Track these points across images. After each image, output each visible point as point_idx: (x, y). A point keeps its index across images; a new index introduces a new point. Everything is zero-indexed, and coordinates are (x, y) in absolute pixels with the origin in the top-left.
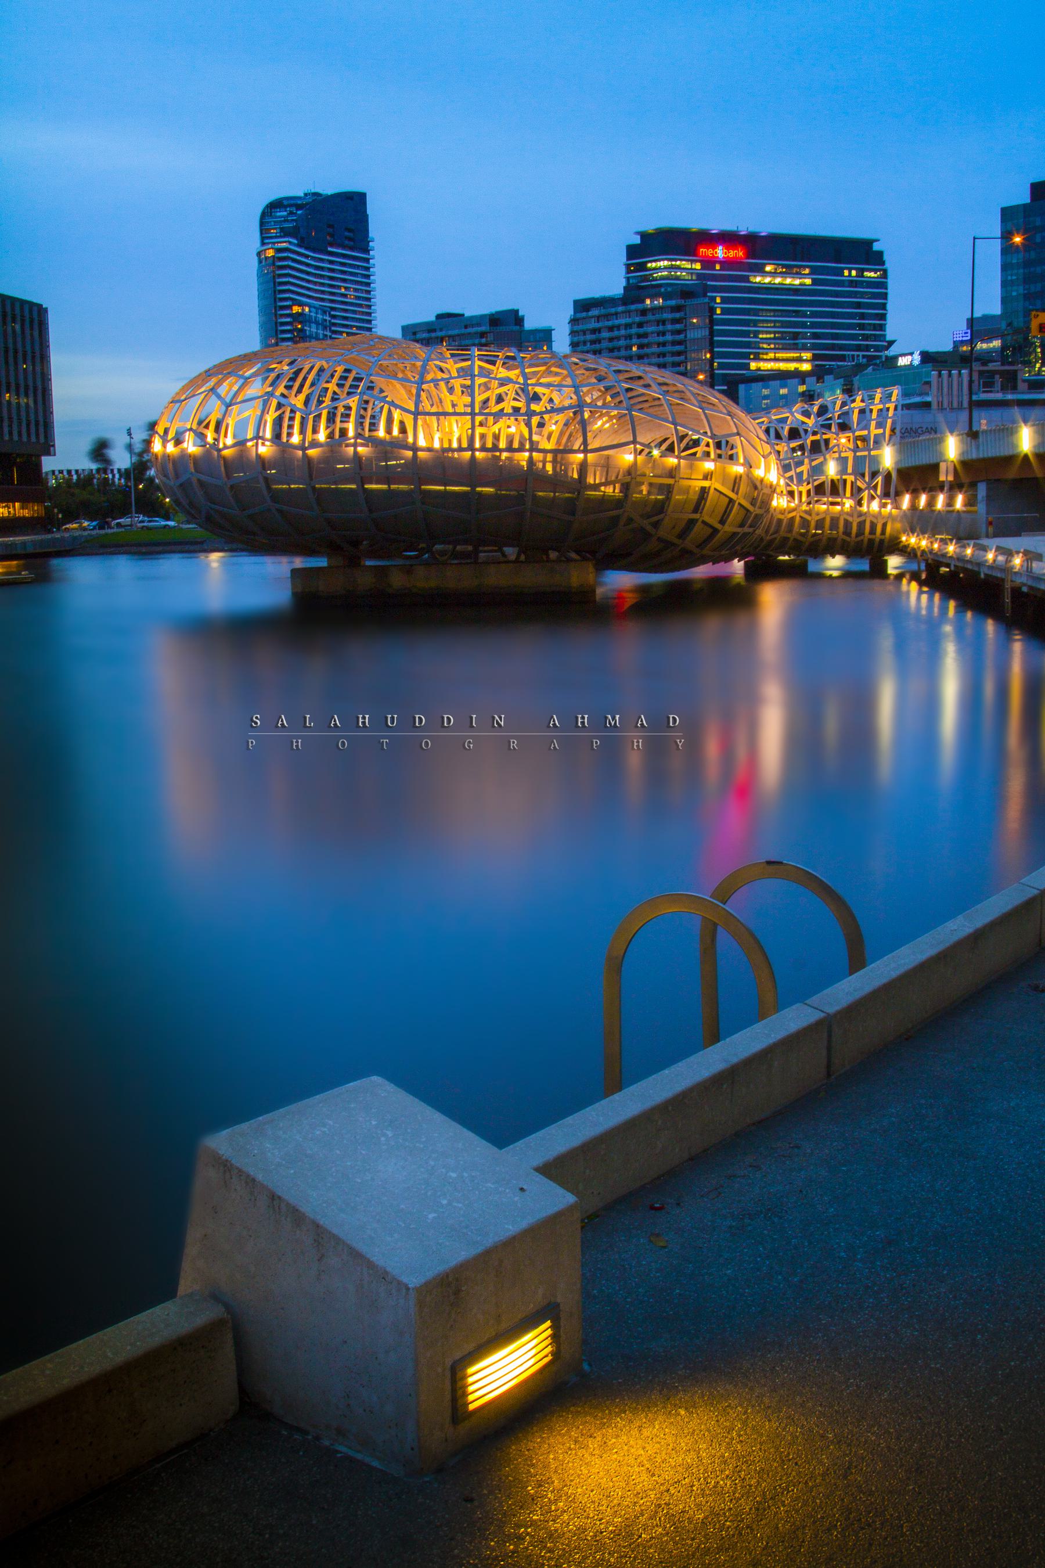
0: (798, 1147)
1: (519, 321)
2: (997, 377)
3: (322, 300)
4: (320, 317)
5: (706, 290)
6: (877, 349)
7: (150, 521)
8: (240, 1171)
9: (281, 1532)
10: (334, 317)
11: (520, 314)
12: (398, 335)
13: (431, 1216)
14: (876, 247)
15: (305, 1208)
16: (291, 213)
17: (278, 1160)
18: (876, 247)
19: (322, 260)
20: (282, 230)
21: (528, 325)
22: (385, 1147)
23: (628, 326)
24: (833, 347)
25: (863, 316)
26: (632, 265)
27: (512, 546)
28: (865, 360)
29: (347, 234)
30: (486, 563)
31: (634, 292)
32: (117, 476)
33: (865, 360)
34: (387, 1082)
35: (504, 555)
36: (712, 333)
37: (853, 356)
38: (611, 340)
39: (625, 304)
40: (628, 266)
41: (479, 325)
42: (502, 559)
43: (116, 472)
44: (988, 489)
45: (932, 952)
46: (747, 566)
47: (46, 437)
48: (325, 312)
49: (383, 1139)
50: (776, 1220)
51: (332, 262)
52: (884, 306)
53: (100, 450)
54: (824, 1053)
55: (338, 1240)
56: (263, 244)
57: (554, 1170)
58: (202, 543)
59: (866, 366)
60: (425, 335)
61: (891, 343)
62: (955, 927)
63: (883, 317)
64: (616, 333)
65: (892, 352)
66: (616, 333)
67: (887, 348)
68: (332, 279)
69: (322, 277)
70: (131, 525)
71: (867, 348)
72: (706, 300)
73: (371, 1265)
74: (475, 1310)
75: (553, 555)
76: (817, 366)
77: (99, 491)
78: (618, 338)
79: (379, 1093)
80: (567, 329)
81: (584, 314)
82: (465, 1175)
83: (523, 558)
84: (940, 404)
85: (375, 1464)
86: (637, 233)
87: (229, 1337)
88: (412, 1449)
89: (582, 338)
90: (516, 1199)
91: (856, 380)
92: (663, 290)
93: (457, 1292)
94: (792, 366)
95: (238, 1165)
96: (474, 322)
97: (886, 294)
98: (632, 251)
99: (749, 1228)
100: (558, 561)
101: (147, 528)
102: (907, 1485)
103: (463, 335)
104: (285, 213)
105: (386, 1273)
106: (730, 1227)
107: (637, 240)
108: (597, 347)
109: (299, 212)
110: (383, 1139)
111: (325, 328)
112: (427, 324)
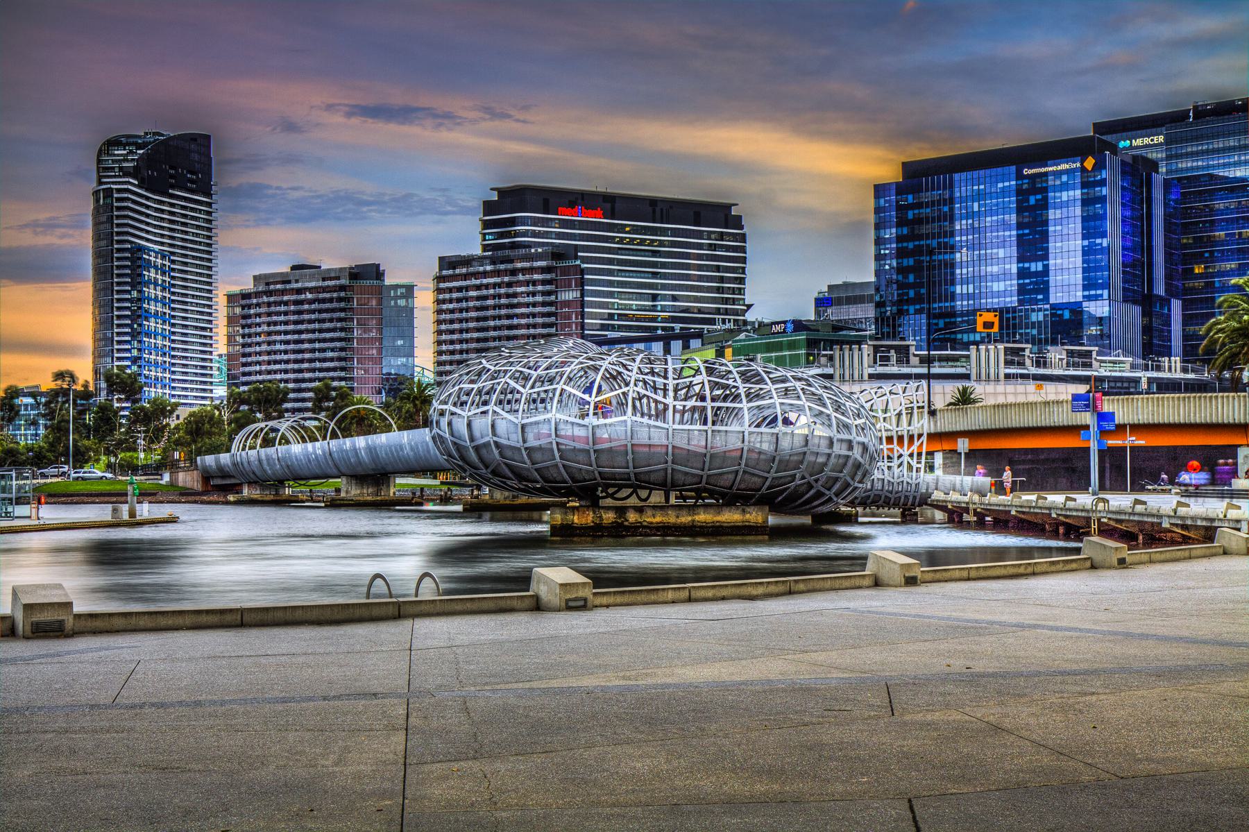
2: (893, 352)
3: (162, 244)
4: (159, 261)
6: (736, 312)
16: (131, 152)
21: (388, 282)
23: (495, 286)
25: (722, 280)
36: (582, 296)
39: (493, 263)
41: (338, 278)
44: (944, 458)
48: (163, 257)
51: (172, 205)
56: (100, 183)
61: (749, 306)
63: (741, 281)
64: (485, 292)
66: (485, 292)
69: (162, 219)
80: (431, 285)
81: (451, 272)
84: (842, 377)
89: (447, 296)
101: (83, 479)
107: (494, 197)
111: (163, 273)
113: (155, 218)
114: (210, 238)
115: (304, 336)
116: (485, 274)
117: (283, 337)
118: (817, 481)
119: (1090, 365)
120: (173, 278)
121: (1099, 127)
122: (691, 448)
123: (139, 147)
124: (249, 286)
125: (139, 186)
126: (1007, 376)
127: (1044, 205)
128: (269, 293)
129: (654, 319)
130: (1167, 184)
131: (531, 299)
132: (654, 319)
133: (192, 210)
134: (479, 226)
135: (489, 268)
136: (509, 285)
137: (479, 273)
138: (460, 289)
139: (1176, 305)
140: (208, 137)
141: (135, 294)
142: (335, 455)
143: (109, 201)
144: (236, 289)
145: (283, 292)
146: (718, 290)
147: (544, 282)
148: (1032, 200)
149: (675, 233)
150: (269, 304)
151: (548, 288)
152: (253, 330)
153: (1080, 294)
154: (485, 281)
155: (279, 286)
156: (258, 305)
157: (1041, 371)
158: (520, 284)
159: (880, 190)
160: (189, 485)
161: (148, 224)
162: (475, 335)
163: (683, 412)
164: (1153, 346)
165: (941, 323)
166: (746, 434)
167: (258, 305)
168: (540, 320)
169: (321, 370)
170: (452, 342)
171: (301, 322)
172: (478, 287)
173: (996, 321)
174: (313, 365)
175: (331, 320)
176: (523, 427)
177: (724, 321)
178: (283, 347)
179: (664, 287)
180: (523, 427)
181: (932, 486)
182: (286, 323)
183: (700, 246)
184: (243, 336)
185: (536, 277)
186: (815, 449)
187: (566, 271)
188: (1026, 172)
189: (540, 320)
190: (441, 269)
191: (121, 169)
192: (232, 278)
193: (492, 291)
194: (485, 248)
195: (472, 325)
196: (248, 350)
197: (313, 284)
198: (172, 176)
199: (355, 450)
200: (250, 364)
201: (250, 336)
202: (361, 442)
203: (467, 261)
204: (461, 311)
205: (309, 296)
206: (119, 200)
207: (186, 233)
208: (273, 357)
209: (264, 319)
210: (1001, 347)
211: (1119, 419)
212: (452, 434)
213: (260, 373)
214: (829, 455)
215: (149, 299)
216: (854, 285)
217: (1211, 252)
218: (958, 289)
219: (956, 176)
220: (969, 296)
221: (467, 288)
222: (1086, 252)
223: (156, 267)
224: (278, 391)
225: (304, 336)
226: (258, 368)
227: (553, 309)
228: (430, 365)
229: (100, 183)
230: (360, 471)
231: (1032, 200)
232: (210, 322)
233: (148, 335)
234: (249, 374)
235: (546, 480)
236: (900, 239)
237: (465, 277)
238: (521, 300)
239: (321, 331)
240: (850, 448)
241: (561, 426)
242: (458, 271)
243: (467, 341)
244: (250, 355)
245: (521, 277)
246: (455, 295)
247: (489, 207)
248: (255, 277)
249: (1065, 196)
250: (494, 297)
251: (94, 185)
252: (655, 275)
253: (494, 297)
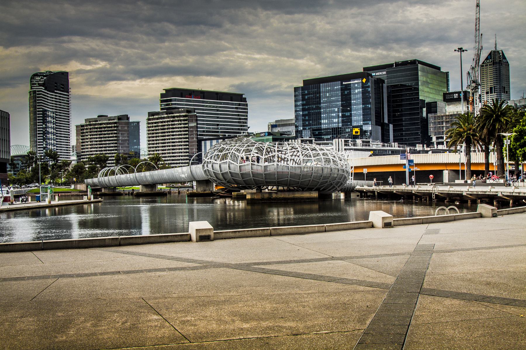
1: (128, 118)
3: (53, 109)
6: (245, 130)
10: (56, 115)
14: (244, 96)
16: (42, 78)
18: (244, 96)
19: (52, 95)
23: (167, 122)
25: (240, 119)
38: (162, 126)
39: (167, 114)
48: (53, 113)
51: (56, 96)
52: (247, 116)
56: (32, 89)
63: (247, 119)
64: (164, 124)
66: (164, 124)
80: (146, 122)
89: (151, 125)
107: (164, 92)
111: (53, 119)
113: (50, 100)
115: (102, 139)
116: (164, 118)
117: (95, 140)
119: (369, 146)
120: (57, 120)
121: (365, 69)
123: (44, 76)
124: (83, 123)
125: (45, 90)
126: (345, 149)
127: (350, 94)
128: (91, 125)
129: (218, 132)
130: (388, 87)
132: (218, 132)
133: (63, 97)
134: (160, 102)
135: (165, 116)
136: (172, 121)
138: (156, 123)
139: (391, 126)
141: (44, 126)
142: (138, 178)
143: (35, 95)
144: (79, 124)
145: (95, 125)
146: (239, 122)
147: (184, 120)
148: (346, 92)
149: (224, 103)
150: (90, 129)
152: (85, 137)
153: (362, 123)
154: (164, 120)
155: (94, 123)
156: (87, 129)
157: (355, 148)
158: (176, 121)
159: (296, 89)
160: (81, 189)
161: (48, 102)
162: (161, 138)
164: (385, 139)
165: (317, 133)
167: (87, 129)
168: (183, 133)
169: (109, 150)
170: (153, 141)
171: (102, 134)
172: (162, 122)
173: (359, 131)
174: (106, 149)
175: (112, 134)
176: (240, 166)
177: (244, 133)
178: (96, 143)
181: (356, 184)
182: (96, 135)
184: (82, 139)
185: (181, 118)
187: (191, 116)
188: (344, 83)
189: (183, 133)
190: (149, 116)
192: (77, 119)
193: (166, 123)
194: (162, 109)
195: (160, 135)
196: (83, 144)
198: (56, 86)
199: (127, 178)
200: (84, 149)
201: (84, 139)
202: (148, 173)
203: (158, 113)
204: (156, 130)
205: (104, 126)
206: (38, 94)
207: (61, 105)
208: (92, 146)
209: (89, 134)
210: (343, 140)
211: (415, 162)
212: (213, 169)
213: (88, 152)
215: (49, 127)
216: (284, 120)
217: (402, 109)
218: (322, 121)
219: (321, 85)
220: (326, 124)
221: (158, 123)
222: (364, 109)
223: (51, 117)
224: (105, 157)
225: (102, 139)
226: (87, 150)
227: (187, 129)
228: (146, 149)
229: (32, 89)
230: (147, 183)
231: (346, 92)
232: (69, 135)
233: (49, 139)
234: (84, 152)
236: (303, 105)
237: (158, 119)
239: (108, 137)
240: (344, 172)
242: (155, 117)
243: (158, 140)
244: (84, 146)
245: (176, 119)
247: (162, 95)
248: (85, 120)
249: (356, 91)
250: (167, 125)
251: (29, 89)
252: (218, 118)
253: (167, 125)
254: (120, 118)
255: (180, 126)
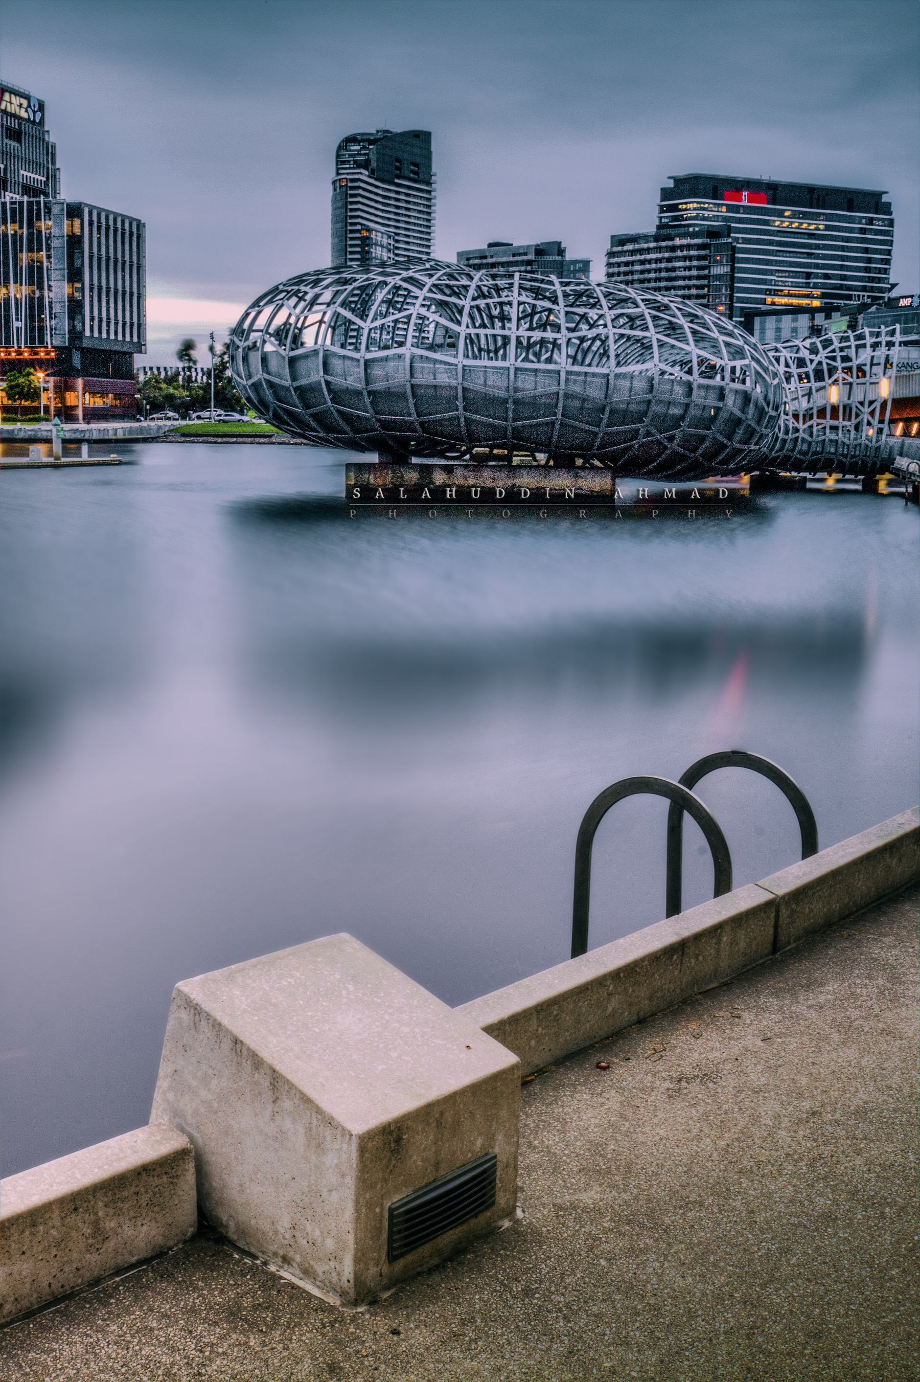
0: (739, 1017)
1: (561, 252)
3: (389, 226)
5: (729, 230)
6: (881, 290)
7: (226, 415)
8: (208, 1015)
9: (220, 1350)
10: (397, 241)
11: (563, 246)
12: (453, 260)
13: (380, 1067)
14: (885, 199)
15: (264, 1054)
16: (364, 148)
17: (244, 1006)
18: (885, 199)
19: (389, 190)
20: (355, 162)
21: (569, 256)
22: (345, 1000)
23: (657, 261)
24: (841, 287)
26: (665, 206)
27: (545, 452)
28: (869, 300)
29: (412, 167)
30: (519, 467)
31: (664, 232)
32: (200, 374)
33: (869, 300)
34: (354, 939)
35: (535, 459)
36: (733, 269)
37: (859, 296)
38: (642, 272)
39: (656, 240)
40: (661, 207)
41: (525, 254)
42: (534, 463)
43: (199, 370)
45: (880, 843)
46: (753, 480)
47: (139, 337)
49: (344, 992)
50: (711, 1085)
51: (398, 193)
53: (186, 350)
54: (771, 931)
55: (291, 1086)
56: (338, 174)
57: (501, 1031)
58: (270, 436)
59: (871, 305)
60: (477, 261)
61: (894, 286)
62: (903, 821)
64: (648, 266)
65: (894, 294)
66: (648, 266)
67: (890, 290)
68: (397, 207)
69: (389, 205)
70: (210, 418)
71: (872, 289)
72: (730, 240)
73: (319, 1111)
74: (415, 1158)
75: (579, 462)
76: (826, 303)
77: (183, 387)
78: (649, 271)
79: (348, 945)
80: (604, 260)
81: (620, 248)
82: (417, 1030)
83: (551, 463)
85: (316, 1292)
86: (670, 178)
87: (191, 1166)
88: (348, 1281)
89: (616, 270)
90: (461, 1056)
91: (860, 317)
92: (691, 229)
93: (398, 1140)
94: (804, 302)
95: (207, 1009)
96: (521, 251)
97: (892, 241)
98: (666, 194)
99: (685, 1091)
100: (583, 468)
101: (224, 421)
102: (805, 1348)
103: (511, 262)
104: (358, 148)
105: (333, 1119)
106: (668, 1089)
107: (671, 184)
108: (630, 278)
109: (371, 147)
110: (344, 992)
112: (480, 251)
114: (429, 220)
116: (648, 250)
118: (671, 439)
122: (489, 391)
131: (687, 273)
134: (657, 209)
136: (669, 260)
137: (643, 249)
138: (627, 264)
140: (428, 134)
146: (867, 270)
147: (699, 258)
151: (703, 263)
158: (677, 259)
163: (529, 346)
166: (612, 377)
172: (643, 262)
179: (817, 266)
180: (367, 363)
183: (851, 230)
185: (692, 253)
186: (666, 397)
187: (719, 248)
190: (612, 247)
191: (355, 162)
193: (653, 266)
197: (504, 259)
198: (397, 168)
214: (687, 406)
221: (633, 263)
227: (706, 282)
235: (357, 431)
238: (678, 273)
241: (418, 365)
242: (625, 248)
245: (679, 253)
246: (623, 269)
250: (656, 271)
251: (332, 175)
252: (810, 255)
254: (540, 251)
255: (687, 273)
